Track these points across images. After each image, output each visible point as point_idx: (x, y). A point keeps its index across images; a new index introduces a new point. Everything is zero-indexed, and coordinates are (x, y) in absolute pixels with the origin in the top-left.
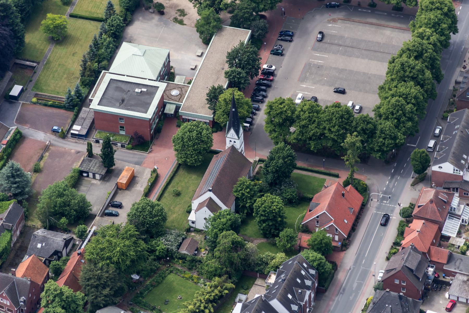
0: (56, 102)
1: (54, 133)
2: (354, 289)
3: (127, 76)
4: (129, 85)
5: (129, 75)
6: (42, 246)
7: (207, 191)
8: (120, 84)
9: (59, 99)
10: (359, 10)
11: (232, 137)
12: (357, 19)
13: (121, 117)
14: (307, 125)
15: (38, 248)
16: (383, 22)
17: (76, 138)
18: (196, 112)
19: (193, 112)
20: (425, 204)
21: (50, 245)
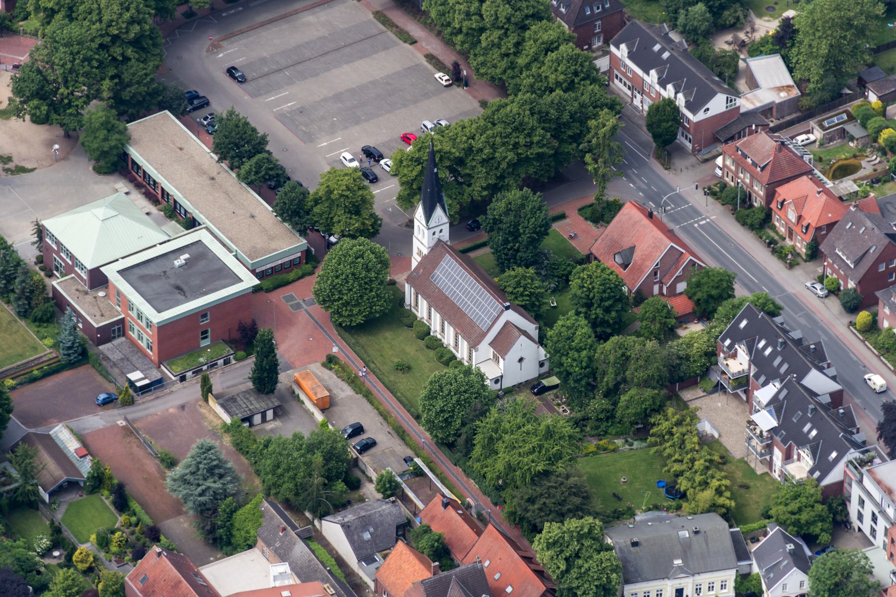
0: (42, 368)
1: (106, 406)
2: (809, 327)
3: (123, 258)
4: (152, 264)
5: (124, 255)
6: (371, 534)
7: (502, 312)
8: (137, 271)
9: (36, 362)
10: (224, 15)
11: (437, 224)
12: (243, 26)
13: (202, 313)
14: (491, 156)
15: (368, 541)
16: (282, 11)
17: (151, 390)
18: (277, 250)
19: (270, 253)
20: (772, 158)
21: (382, 524)
